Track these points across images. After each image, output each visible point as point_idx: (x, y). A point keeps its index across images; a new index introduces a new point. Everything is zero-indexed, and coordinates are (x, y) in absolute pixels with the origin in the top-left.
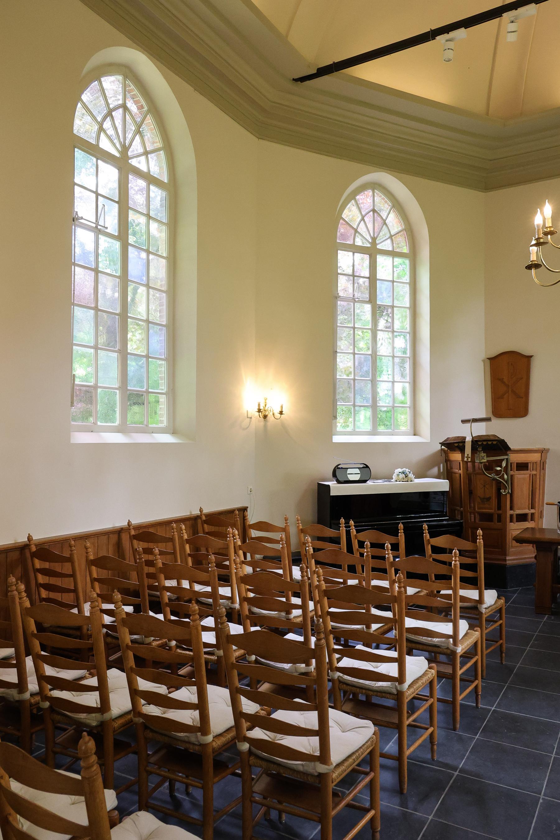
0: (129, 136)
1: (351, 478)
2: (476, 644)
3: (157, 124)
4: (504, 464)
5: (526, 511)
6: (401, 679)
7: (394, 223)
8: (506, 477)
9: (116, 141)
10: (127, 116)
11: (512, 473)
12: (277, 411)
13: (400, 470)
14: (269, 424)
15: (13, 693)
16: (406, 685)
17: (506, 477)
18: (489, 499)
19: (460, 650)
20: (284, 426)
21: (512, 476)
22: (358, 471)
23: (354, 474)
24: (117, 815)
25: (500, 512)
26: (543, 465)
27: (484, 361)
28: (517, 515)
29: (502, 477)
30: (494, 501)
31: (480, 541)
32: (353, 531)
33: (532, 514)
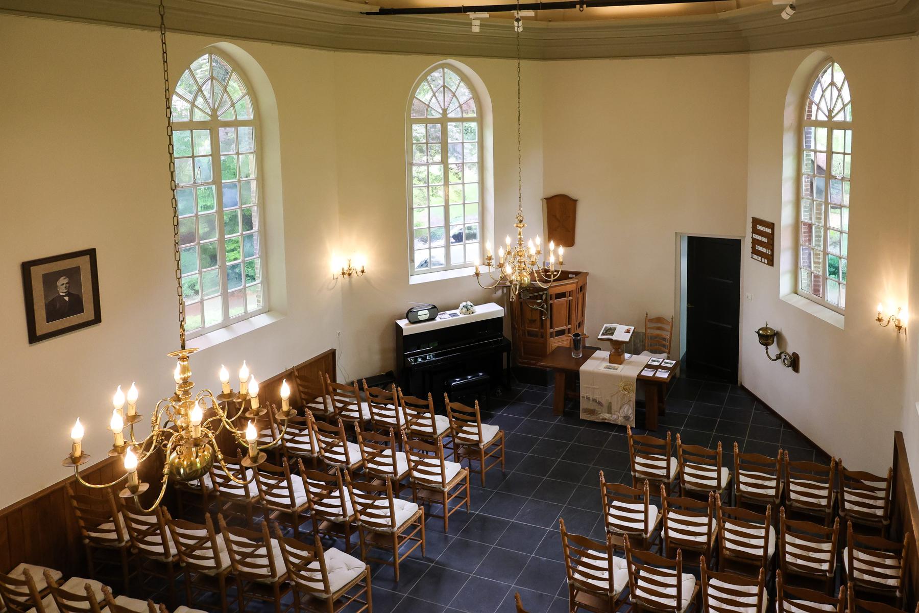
1: (421, 318)
2: (466, 477)
3: (243, 80)
4: (544, 297)
5: (564, 327)
6: (393, 525)
7: (464, 93)
10: (216, 88)
11: (551, 302)
12: (359, 269)
13: (464, 304)
14: (353, 280)
15: (163, 558)
16: (396, 529)
19: (446, 490)
20: (367, 280)
22: (427, 312)
23: (423, 314)
26: (582, 289)
30: (538, 323)
31: (477, 407)
32: (401, 394)
33: (569, 329)
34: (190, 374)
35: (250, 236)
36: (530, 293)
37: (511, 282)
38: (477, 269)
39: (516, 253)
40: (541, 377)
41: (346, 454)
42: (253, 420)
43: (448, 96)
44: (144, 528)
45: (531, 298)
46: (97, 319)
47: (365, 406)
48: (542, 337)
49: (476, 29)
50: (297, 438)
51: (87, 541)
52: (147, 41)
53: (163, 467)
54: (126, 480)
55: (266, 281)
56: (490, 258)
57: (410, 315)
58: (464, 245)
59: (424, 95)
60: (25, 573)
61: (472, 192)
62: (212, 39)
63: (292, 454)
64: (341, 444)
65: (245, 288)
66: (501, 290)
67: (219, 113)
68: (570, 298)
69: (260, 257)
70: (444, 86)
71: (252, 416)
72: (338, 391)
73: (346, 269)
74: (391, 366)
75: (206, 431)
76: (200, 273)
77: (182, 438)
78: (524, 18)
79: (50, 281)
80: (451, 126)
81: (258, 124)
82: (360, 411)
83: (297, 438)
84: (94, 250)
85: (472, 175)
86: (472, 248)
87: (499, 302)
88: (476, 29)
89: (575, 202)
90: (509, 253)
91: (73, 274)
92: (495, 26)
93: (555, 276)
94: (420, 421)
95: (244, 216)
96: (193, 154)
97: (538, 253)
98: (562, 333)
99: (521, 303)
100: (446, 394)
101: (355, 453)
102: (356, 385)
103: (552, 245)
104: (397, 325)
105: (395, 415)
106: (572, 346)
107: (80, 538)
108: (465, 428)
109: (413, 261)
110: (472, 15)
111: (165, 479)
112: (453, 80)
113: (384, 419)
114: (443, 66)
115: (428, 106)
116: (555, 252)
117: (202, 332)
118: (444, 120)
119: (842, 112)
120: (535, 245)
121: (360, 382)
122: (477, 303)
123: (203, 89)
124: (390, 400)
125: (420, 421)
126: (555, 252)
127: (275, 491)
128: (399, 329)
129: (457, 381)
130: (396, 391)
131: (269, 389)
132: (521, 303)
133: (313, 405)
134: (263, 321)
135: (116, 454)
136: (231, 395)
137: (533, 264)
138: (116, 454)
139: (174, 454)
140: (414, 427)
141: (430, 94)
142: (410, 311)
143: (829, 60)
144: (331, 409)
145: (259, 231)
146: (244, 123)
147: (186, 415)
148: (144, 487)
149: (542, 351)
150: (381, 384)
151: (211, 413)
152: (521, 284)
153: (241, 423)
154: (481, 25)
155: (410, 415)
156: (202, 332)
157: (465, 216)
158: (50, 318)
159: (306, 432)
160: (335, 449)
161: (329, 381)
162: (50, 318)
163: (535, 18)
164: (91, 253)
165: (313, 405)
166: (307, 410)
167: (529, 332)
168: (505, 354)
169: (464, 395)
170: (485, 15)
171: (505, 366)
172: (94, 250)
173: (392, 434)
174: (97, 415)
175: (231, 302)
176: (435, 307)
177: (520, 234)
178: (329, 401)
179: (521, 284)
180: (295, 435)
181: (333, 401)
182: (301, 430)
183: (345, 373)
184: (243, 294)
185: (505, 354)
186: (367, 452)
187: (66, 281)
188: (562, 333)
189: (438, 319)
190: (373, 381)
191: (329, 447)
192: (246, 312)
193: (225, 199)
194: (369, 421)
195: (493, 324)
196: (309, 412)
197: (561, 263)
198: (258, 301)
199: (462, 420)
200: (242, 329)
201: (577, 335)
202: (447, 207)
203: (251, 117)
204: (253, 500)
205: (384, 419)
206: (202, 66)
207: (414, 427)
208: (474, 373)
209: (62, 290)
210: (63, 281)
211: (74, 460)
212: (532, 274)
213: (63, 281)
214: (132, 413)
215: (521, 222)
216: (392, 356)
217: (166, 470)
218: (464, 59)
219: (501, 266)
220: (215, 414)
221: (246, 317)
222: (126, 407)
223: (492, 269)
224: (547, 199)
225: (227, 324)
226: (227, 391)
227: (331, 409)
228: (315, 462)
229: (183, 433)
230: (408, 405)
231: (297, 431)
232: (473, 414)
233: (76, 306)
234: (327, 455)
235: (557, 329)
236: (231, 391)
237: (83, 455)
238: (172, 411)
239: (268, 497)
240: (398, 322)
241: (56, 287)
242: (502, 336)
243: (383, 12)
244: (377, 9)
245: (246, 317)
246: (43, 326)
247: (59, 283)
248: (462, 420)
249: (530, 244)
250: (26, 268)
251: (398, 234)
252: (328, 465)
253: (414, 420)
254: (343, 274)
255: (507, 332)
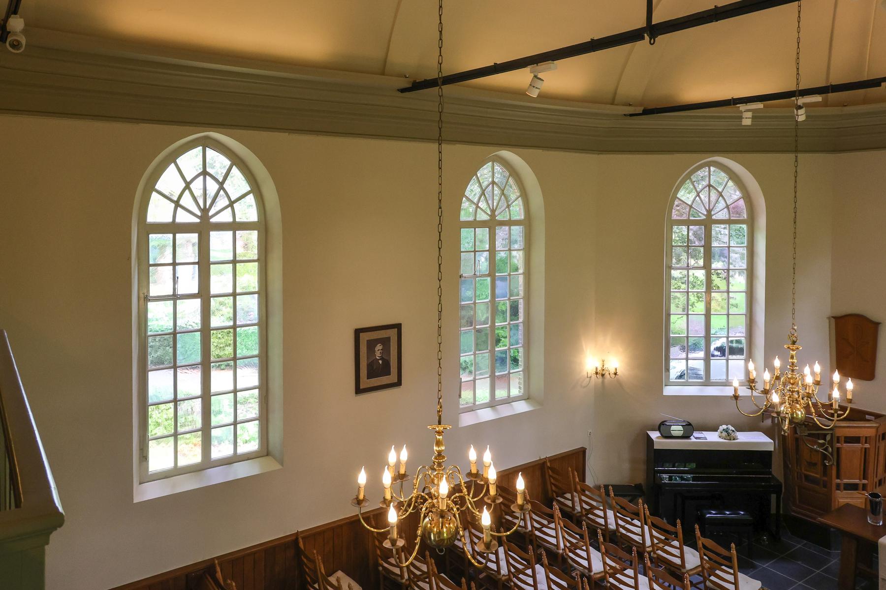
0: (496, 198)
1: (674, 433)
4: (828, 438)
5: (857, 481)
7: (733, 194)
8: (830, 449)
9: (490, 202)
11: (839, 445)
12: (612, 371)
13: (724, 427)
17: (830, 449)
18: (815, 464)
21: (838, 449)
22: (680, 428)
23: (677, 430)
24: (855, 385)
25: (825, 478)
27: (829, 318)
28: (845, 484)
29: (826, 449)
32: (648, 513)
33: (864, 485)
34: (443, 448)
35: (517, 325)
36: (806, 430)
37: (778, 413)
38: (736, 390)
39: (786, 380)
40: (823, 537)
41: (588, 559)
42: (489, 506)
43: (714, 195)
44: (418, 573)
45: (809, 435)
46: (399, 383)
47: (610, 514)
48: (825, 486)
49: (747, 122)
50: (544, 529)
51: (381, 568)
52: (419, 154)
53: (417, 529)
54: (388, 532)
55: (527, 371)
56: (753, 381)
57: (663, 427)
58: (727, 360)
59: (685, 195)
60: (338, 580)
61: (740, 299)
62: (191, 128)
63: (538, 544)
64: (584, 548)
65: (509, 373)
66: (765, 419)
67: (496, 213)
68: (867, 446)
69: (523, 346)
70: (710, 186)
71: (489, 501)
72: (587, 493)
73: (599, 369)
74: (640, 478)
75: (452, 505)
76: (475, 354)
77: (433, 506)
78: (806, 105)
79: (371, 344)
80: (716, 229)
81: (527, 223)
82: (605, 518)
83: (544, 529)
84: (400, 324)
85: (739, 282)
86: (737, 364)
87: (768, 433)
88: (747, 122)
89: (876, 325)
90: (778, 378)
91: (386, 342)
92: (770, 117)
93: (839, 416)
94: (666, 548)
95: (511, 307)
96: (473, 250)
97: (817, 383)
98: (854, 487)
99: (797, 440)
100: (697, 526)
101: (597, 563)
102: (602, 490)
103: (837, 377)
104: (648, 437)
105: (640, 532)
106: (869, 507)
107: (377, 565)
108: (718, 572)
109: (668, 370)
110: (742, 107)
111: (418, 540)
112: (718, 177)
113: (629, 534)
114: (709, 165)
115: (691, 207)
116: (842, 387)
117: (473, 408)
118: (708, 223)
119: (187, 191)
120: (813, 373)
121: (606, 487)
122: (740, 429)
123: (191, 186)
124: (636, 515)
125: (666, 548)
126: (842, 387)
127: (521, 576)
128: (650, 441)
129: (712, 514)
130: (642, 506)
131: (506, 478)
132: (797, 440)
133: (562, 500)
134: (522, 407)
135: (385, 506)
136: (477, 475)
137: (809, 396)
138: (385, 506)
139: (427, 519)
140: (659, 552)
141: (694, 194)
142: (663, 423)
143: (206, 143)
144: (578, 508)
145: (523, 322)
146: (246, 226)
147: (438, 485)
148: (401, 543)
149: (825, 506)
150: (629, 495)
151: (456, 489)
152: (793, 417)
153: (479, 505)
154: (753, 118)
155: (657, 538)
156: (473, 408)
157: (728, 326)
158: (369, 376)
159: (552, 525)
160: (578, 551)
161: (577, 480)
162: (369, 376)
163: (825, 104)
164: (398, 327)
165: (562, 500)
166: (554, 503)
167: (807, 477)
168: (773, 497)
169: (721, 533)
170: (760, 105)
171: (773, 511)
172: (400, 324)
173: (634, 554)
174: (376, 465)
175: (497, 383)
176: (690, 424)
177: (792, 357)
178: (577, 499)
179: (793, 417)
180: (543, 525)
181: (581, 500)
182: (549, 523)
183: (596, 473)
184: (507, 378)
185: (773, 497)
186: (609, 566)
187: (381, 348)
188: (854, 487)
189: (693, 439)
190: (621, 490)
191: (573, 548)
192: (509, 396)
193: (497, 291)
194: (614, 532)
195: (760, 457)
196: (556, 506)
197: (850, 401)
198: (520, 388)
199: (715, 562)
200: (505, 411)
201: (875, 495)
202: (708, 315)
203: (523, 217)
204: (504, 578)
205: (629, 534)
206: (485, 173)
207: (659, 552)
208: (734, 509)
209: (378, 355)
210: (379, 347)
211: (359, 502)
212: (807, 407)
213: (379, 347)
214: (402, 471)
215: (794, 343)
216: (642, 467)
217: (419, 532)
218: (731, 155)
219: (766, 392)
220: (461, 491)
221: (509, 401)
222: (398, 464)
223: (755, 393)
224: (836, 318)
225: (493, 404)
226: (474, 471)
227: (578, 508)
228: (560, 559)
229: (435, 501)
230: (654, 526)
231: (545, 522)
232: (729, 559)
233: (385, 369)
234: (571, 555)
235: (846, 481)
236: (478, 471)
237: (364, 500)
238: (429, 480)
239: (515, 580)
240: (649, 433)
241: (374, 351)
242: (770, 473)
243: (647, 112)
244: (640, 110)
245: (509, 401)
246: (365, 383)
247: (376, 349)
248: (715, 562)
249: (807, 370)
250: (358, 332)
251: (653, 340)
252: (572, 566)
253: (661, 545)
254: (597, 373)
255: (777, 470)
